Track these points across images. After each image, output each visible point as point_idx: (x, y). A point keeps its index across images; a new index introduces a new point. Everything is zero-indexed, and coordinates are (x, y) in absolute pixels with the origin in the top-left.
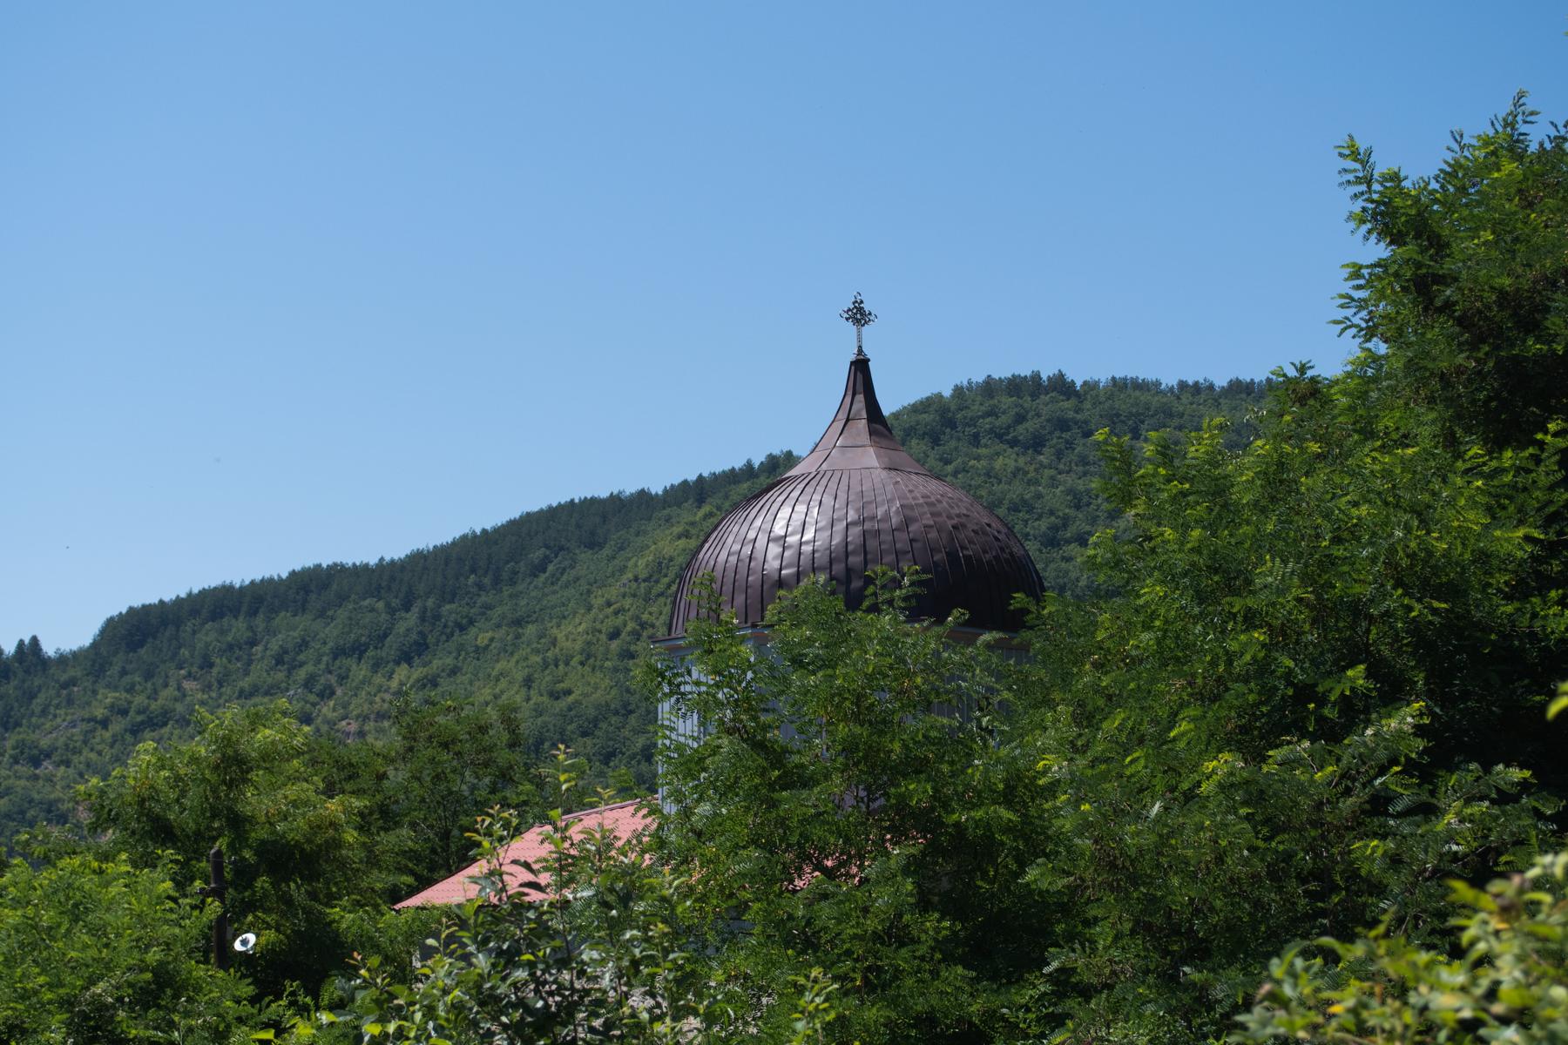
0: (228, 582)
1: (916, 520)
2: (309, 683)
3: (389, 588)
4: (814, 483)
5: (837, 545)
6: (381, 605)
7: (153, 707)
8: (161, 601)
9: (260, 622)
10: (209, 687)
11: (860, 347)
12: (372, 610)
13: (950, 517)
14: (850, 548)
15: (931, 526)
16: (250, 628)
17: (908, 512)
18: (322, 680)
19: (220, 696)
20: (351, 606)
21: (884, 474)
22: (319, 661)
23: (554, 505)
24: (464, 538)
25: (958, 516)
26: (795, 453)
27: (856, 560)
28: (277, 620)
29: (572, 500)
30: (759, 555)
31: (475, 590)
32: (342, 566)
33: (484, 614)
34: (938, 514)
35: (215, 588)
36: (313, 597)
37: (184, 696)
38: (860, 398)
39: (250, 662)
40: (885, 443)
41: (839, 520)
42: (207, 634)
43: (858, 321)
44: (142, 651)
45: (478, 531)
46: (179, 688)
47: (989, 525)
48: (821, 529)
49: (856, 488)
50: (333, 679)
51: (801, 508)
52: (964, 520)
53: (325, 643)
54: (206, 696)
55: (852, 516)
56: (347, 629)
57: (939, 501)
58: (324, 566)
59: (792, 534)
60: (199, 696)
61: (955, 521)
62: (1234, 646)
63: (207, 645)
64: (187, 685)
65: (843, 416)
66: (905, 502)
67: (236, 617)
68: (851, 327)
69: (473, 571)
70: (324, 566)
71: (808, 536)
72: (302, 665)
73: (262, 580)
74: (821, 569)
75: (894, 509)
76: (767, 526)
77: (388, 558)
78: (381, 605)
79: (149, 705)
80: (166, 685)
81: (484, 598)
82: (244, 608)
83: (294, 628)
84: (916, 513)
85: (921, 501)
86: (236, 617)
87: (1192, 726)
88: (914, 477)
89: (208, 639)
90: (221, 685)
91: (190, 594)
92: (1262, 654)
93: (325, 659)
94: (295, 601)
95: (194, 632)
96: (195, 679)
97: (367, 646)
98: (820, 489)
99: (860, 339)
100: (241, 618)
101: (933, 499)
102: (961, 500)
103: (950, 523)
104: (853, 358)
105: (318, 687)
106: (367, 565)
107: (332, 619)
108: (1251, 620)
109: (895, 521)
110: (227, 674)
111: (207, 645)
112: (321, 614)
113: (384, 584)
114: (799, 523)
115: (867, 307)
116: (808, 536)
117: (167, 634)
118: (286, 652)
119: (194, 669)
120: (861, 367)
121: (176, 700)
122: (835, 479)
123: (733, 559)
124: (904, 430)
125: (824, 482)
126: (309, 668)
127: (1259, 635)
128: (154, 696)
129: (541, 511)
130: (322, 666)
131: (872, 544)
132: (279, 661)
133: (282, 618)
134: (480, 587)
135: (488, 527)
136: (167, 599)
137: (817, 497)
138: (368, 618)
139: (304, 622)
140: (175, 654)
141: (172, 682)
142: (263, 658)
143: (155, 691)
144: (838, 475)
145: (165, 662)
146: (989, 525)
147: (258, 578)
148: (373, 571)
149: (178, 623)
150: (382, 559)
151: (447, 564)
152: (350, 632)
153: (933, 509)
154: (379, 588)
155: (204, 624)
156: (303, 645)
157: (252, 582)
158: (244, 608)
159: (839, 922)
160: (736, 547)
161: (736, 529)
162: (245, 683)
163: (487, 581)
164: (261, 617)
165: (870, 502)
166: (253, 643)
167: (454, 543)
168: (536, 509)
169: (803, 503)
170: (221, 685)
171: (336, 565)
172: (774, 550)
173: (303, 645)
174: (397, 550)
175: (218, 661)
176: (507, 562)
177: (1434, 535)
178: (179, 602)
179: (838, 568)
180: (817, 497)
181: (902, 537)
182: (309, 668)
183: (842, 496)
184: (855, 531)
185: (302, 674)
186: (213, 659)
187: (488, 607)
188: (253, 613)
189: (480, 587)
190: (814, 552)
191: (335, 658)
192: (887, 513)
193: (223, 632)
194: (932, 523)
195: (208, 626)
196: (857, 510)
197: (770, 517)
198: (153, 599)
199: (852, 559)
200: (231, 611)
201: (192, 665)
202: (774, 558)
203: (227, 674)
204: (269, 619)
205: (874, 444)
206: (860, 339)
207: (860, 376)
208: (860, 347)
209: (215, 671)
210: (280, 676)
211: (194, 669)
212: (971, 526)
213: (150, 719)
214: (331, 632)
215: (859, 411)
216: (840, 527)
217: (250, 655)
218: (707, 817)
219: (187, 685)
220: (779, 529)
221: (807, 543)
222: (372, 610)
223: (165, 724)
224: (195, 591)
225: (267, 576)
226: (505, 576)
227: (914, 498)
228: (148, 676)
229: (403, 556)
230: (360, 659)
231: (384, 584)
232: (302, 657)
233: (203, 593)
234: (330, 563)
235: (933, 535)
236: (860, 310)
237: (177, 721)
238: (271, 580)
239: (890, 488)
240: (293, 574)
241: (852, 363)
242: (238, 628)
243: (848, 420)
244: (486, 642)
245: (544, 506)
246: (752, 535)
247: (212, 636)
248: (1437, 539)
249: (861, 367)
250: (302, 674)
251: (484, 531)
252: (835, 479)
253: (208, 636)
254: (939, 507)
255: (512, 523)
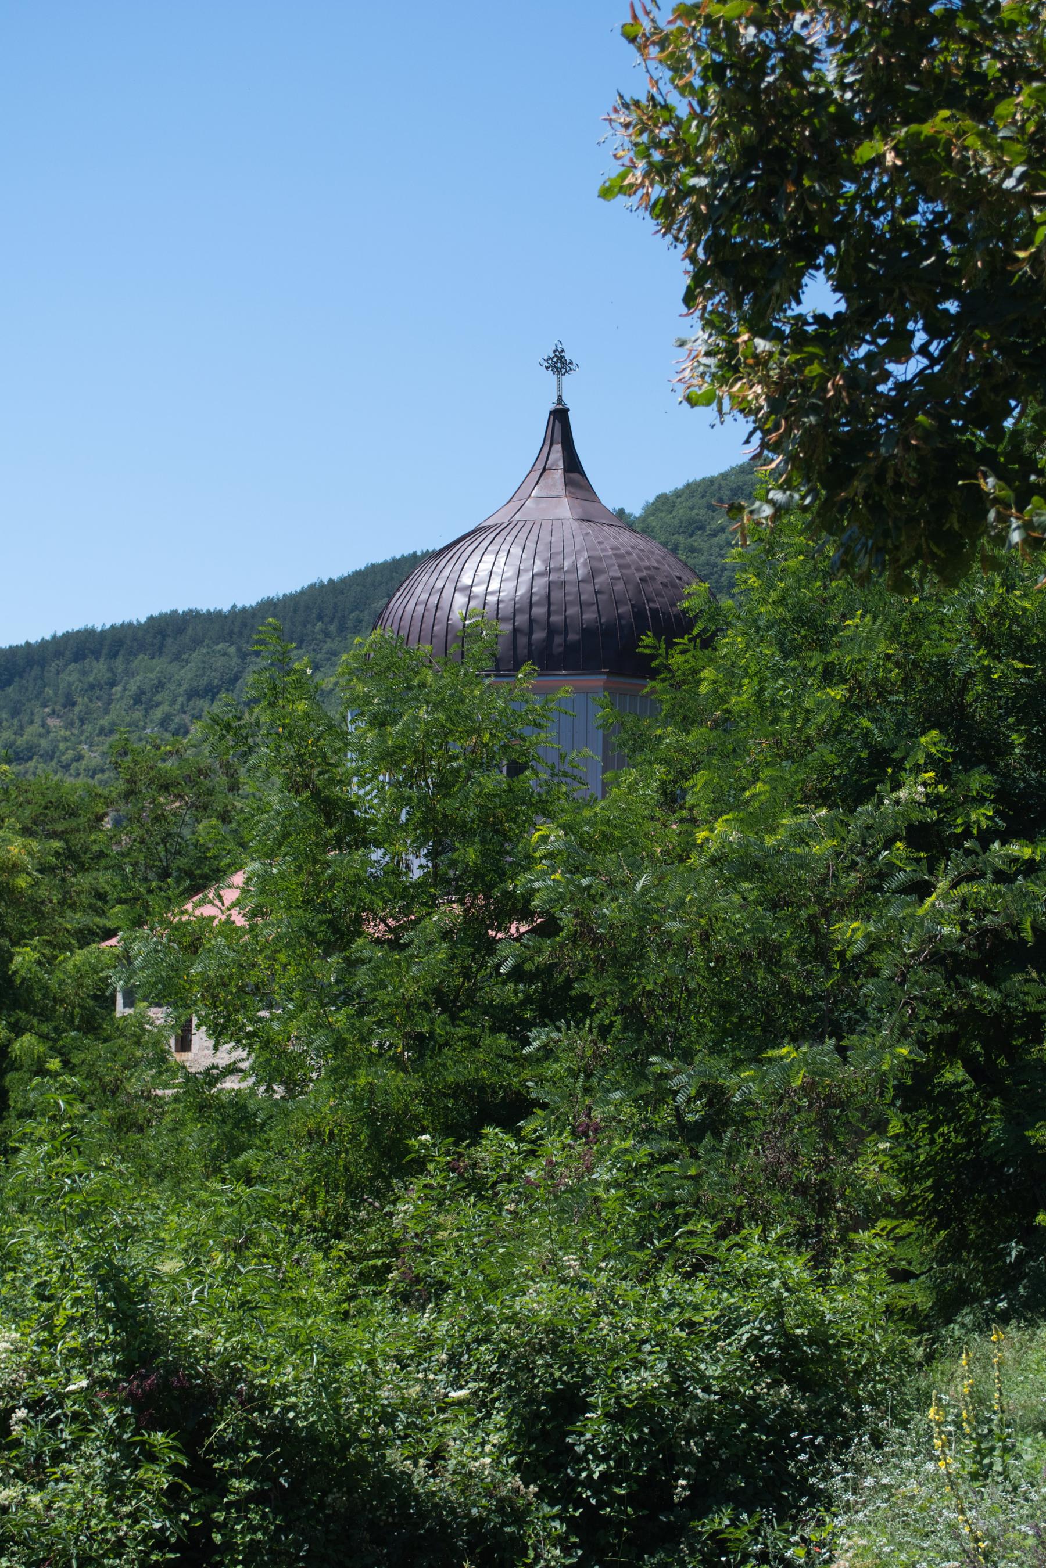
0: (90, 626)
1: (601, 572)
2: (164, 723)
3: (241, 634)
4: (504, 533)
5: (522, 596)
6: (232, 650)
7: (19, 742)
8: (28, 643)
9: (119, 664)
10: (72, 724)
11: (560, 397)
12: (225, 654)
13: (638, 569)
14: (535, 599)
15: (619, 579)
16: (110, 670)
17: (596, 564)
18: (177, 720)
19: (82, 733)
20: (205, 651)
21: (575, 525)
22: (174, 702)
23: (398, 557)
24: (312, 587)
25: (648, 568)
26: (627, 511)
27: (539, 611)
28: (136, 662)
29: (415, 553)
30: (445, 604)
31: (321, 637)
32: (197, 612)
33: (329, 659)
34: (627, 566)
35: (78, 632)
36: (169, 640)
37: (49, 732)
38: (558, 448)
39: (109, 702)
40: (580, 494)
41: (526, 571)
42: (70, 675)
43: (559, 370)
44: (10, 690)
45: (325, 581)
46: (43, 725)
47: (680, 578)
48: (507, 580)
49: (545, 537)
50: (187, 718)
51: (489, 558)
52: (652, 572)
53: (180, 685)
54: (68, 733)
55: (539, 566)
56: (200, 672)
57: (629, 553)
58: (180, 612)
59: (478, 584)
60: (62, 732)
61: (644, 573)
62: (808, 703)
63: (70, 685)
64: (52, 722)
65: (540, 466)
66: (591, 553)
67: (97, 659)
68: (551, 376)
69: (320, 618)
70: (180, 612)
71: (494, 586)
72: (158, 704)
73: (123, 625)
74: (505, 619)
75: (581, 560)
76: (454, 576)
77: (239, 606)
78: (232, 650)
79: (15, 741)
80: (32, 722)
81: (329, 645)
82: (105, 651)
83: (152, 671)
84: (604, 565)
85: (610, 552)
86: (97, 659)
87: (767, 788)
88: (606, 528)
89: (71, 679)
90: (82, 722)
91: (54, 637)
92: (838, 714)
93: (180, 699)
94: (153, 645)
95: (58, 673)
96: (58, 717)
97: (219, 688)
98: (510, 539)
99: (560, 389)
100: (102, 660)
101: (623, 551)
102: (652, 553)
103: (638, 575)
104: (552, 407)
105: (172, 727)
106: (220, 611)
107: (187, 662)
108: (830, 675)
109: (582, 572)
110: (89, 712)
111: (70, 685)
112: (177, 657)
113: (236, 630)
114: (486, 573)
115: (568, 356)
116: (494, 586)
117: (33, 674)
118: (143, 693)
119: (58, 707)
120: (560, 416)
121: (40, 736)
122: (526, 529)
123: (420, 608)
124: (732, 490)
125: (514, 532)
126: (165, 708)
127: (838, 693)
128: (20, 731)
129: (385, 563)
130: (177, 707)
131: (557, 595)
132: (137, 700)
133: (141, 660)
134: (327, 634)
135: (335, 577)
136: (32, 641)
137: (505, 547)
138: (221, 661)
139: (160, 665)
140: (41, 693)
141: (37, 720)
142: (122, 698)
143: (22, 728)
144: (529, 525)
145: (29, 700)
146: (680, 578)
147: (118, 622)
148: (226, 617)
149: (43, 663)
150: (234, 606)
151: (295, 611)
152: (202, 676)
153: (622, 561)
154: (231, 633)
155: (66, 665)
156: (160, 686)
157: (112, 627)
158: (105, 651)
159: (374, 989)
160: (425, 596)
161: (425, 579)
162: (105, 721)
163: (332, 628)
164: (120, 658)
165: (558, 553)
166: (112, 684)
167: (303, 592)
168: (380, 561)
169: (491, 552)
170: (82, 722)
171: (191, 611)
172: (460, 599)
173: (160, 686)
174: (249, 599)
175: (80, 700)
176: (352, 611)
177: (1018, 593)
178: (43, 643)
179: (522, 619)
180: (505, 547)
181: (587, 588)
182: (165, 708)
183: (531, 545)
184: (541, 583)
185: (158, 714)
186: (76, 698)
187: (335, 654)
188: (114, 655)
189: (327, 634)
190: (498, 602)
191: (189, 699)
192: (575, 564)
193: (84, 673)
194: (619, 575)
195: (71, 667)
196: (544, 561)
197: (458, 566)
198: (20, 641)
199: (535, 610)
200: (93, 653)
201: (55, 703)
202: (461, 608)
203: (89, 712)
204: (128, 662)
205: (571, 495)
206: (560, 389)
207: (558, 425)
208: (560, 397)
209: (77, 709)
210: (138, 715)
211: (58, 707)
212: (660, 579)
213: (16, 753)
214: (186, 675)
215: (555, 462)
216: (526, 577)
217: (110, 695)
218: (258, 876)
219: (52, 722)
220: (466, 580)
221: (492, 593)
222: (225, 654)
223: (30, 758)
224: (59, 634)
225: (127, 621)
226: (350, 624)
227: (603, 550)
228: (15, 712)
229: (254, 604)
230: (212, 701)
231: (236, 630)
232: (158, 698)
233: (67, 636)
234: (186, 609)
235: (619, 587)
236: (561, 358)
237: (41, 756)
238: (131, 624)
239: (579, 539)
240: (151, 618)
241: (551, 412)
242: (99, 669)
243: (544, 470)
244: (331, 686)
245: (388, 558)
246: (439, 585)
247: (76, 676)
248: (1020, 598)
249: (560, 416)
250: (158, 714)
251: (331, 581)
252: (526, 529)
253: (71, 676)
254: (628, 559)
255: (358, 574)
